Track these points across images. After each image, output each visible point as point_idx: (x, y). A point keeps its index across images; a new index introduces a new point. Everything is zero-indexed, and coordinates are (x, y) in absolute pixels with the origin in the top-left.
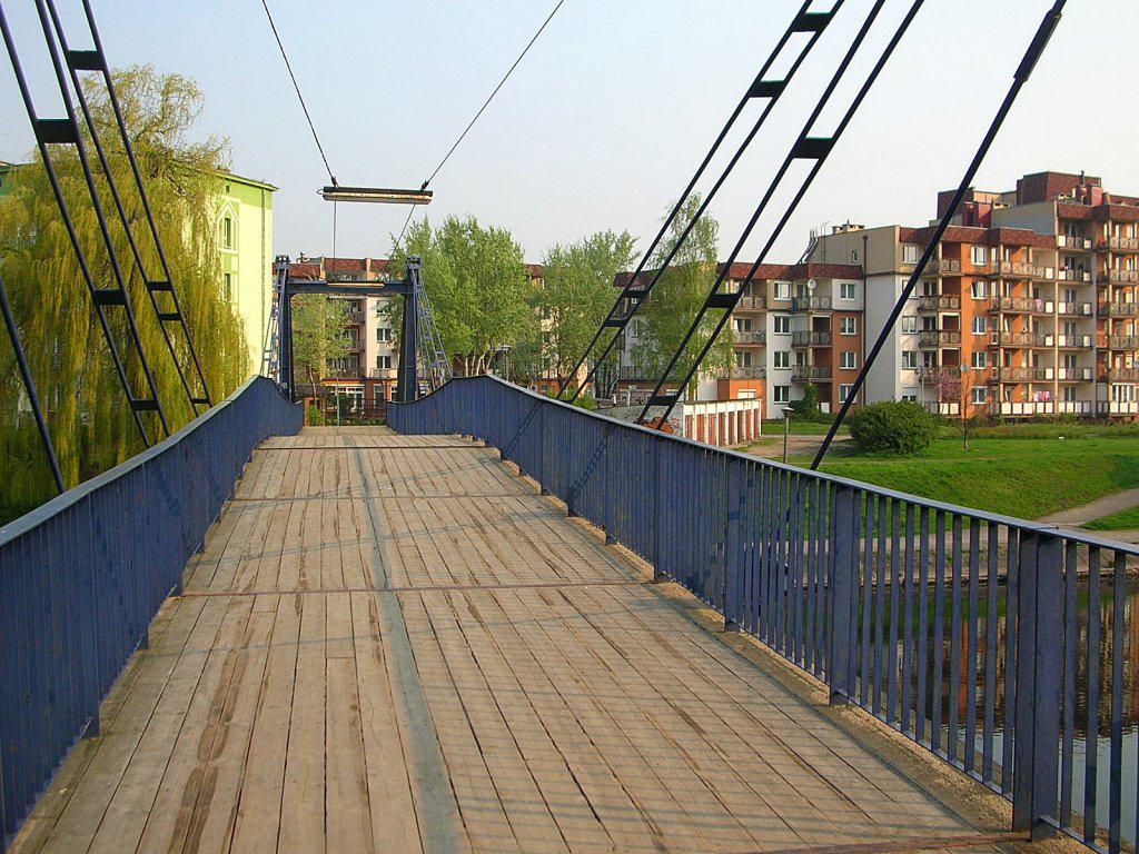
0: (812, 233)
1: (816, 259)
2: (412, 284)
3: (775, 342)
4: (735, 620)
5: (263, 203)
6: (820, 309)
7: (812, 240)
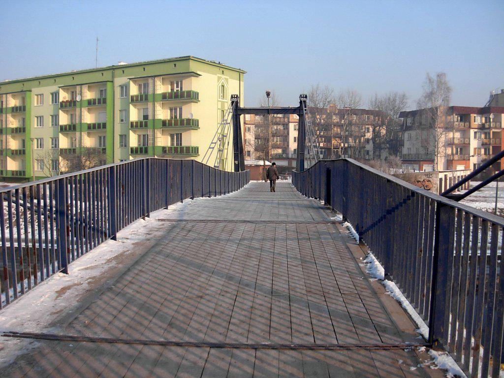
0: (491, 93)
1: (493, 105)
2: (302, 109)
3: (474, 143)
4: (389, 274)
5: (154, 122)
6: (496, 128)
7: (491, 96)
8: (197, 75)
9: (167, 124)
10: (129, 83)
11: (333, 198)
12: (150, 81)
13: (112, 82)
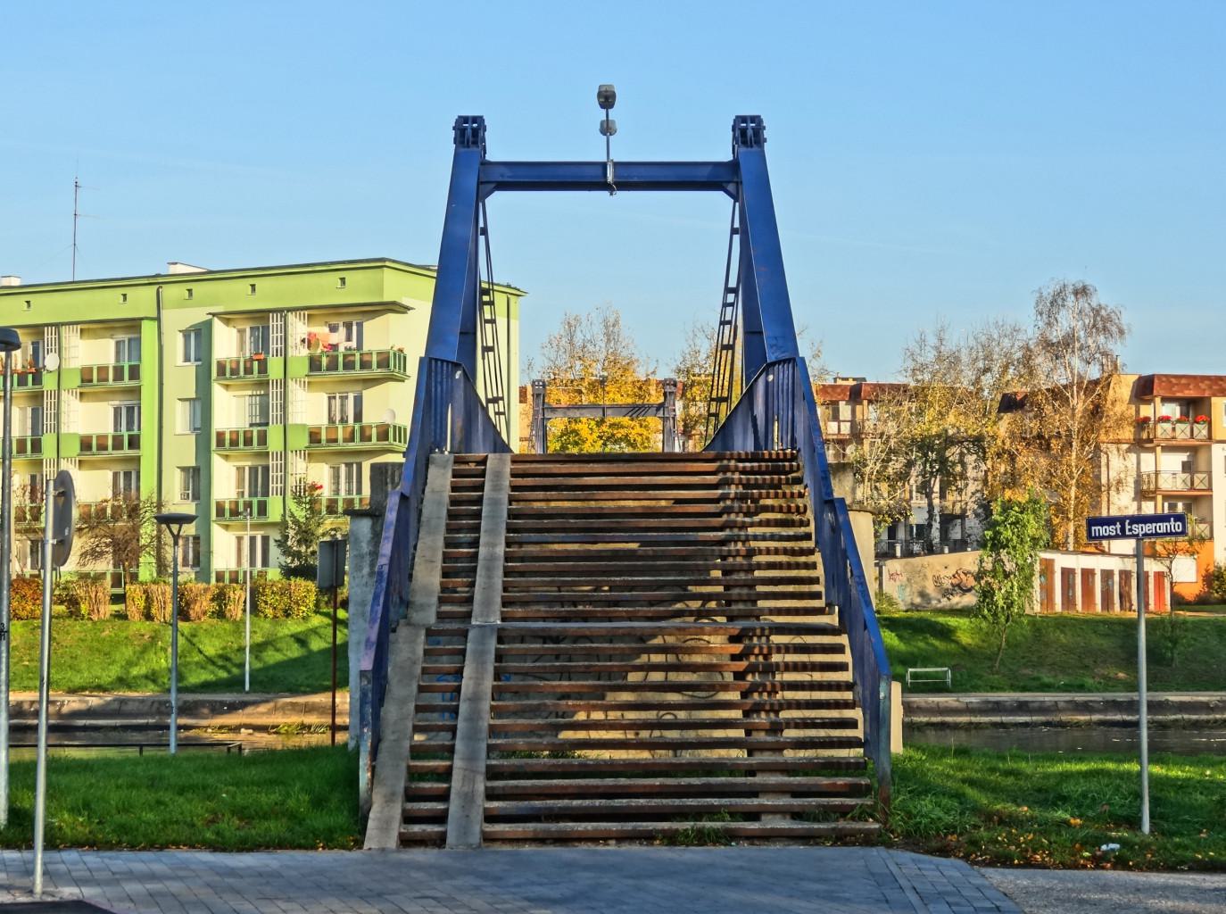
8: (402, 310)
9: (324, 437)
10: (209, 324)
11: (623, 177)
12: (274, 322)
13: (158, 319)
